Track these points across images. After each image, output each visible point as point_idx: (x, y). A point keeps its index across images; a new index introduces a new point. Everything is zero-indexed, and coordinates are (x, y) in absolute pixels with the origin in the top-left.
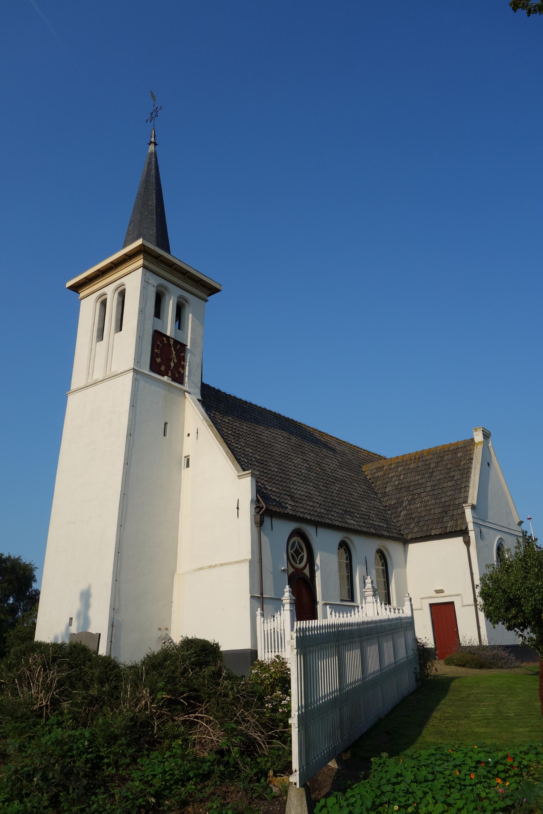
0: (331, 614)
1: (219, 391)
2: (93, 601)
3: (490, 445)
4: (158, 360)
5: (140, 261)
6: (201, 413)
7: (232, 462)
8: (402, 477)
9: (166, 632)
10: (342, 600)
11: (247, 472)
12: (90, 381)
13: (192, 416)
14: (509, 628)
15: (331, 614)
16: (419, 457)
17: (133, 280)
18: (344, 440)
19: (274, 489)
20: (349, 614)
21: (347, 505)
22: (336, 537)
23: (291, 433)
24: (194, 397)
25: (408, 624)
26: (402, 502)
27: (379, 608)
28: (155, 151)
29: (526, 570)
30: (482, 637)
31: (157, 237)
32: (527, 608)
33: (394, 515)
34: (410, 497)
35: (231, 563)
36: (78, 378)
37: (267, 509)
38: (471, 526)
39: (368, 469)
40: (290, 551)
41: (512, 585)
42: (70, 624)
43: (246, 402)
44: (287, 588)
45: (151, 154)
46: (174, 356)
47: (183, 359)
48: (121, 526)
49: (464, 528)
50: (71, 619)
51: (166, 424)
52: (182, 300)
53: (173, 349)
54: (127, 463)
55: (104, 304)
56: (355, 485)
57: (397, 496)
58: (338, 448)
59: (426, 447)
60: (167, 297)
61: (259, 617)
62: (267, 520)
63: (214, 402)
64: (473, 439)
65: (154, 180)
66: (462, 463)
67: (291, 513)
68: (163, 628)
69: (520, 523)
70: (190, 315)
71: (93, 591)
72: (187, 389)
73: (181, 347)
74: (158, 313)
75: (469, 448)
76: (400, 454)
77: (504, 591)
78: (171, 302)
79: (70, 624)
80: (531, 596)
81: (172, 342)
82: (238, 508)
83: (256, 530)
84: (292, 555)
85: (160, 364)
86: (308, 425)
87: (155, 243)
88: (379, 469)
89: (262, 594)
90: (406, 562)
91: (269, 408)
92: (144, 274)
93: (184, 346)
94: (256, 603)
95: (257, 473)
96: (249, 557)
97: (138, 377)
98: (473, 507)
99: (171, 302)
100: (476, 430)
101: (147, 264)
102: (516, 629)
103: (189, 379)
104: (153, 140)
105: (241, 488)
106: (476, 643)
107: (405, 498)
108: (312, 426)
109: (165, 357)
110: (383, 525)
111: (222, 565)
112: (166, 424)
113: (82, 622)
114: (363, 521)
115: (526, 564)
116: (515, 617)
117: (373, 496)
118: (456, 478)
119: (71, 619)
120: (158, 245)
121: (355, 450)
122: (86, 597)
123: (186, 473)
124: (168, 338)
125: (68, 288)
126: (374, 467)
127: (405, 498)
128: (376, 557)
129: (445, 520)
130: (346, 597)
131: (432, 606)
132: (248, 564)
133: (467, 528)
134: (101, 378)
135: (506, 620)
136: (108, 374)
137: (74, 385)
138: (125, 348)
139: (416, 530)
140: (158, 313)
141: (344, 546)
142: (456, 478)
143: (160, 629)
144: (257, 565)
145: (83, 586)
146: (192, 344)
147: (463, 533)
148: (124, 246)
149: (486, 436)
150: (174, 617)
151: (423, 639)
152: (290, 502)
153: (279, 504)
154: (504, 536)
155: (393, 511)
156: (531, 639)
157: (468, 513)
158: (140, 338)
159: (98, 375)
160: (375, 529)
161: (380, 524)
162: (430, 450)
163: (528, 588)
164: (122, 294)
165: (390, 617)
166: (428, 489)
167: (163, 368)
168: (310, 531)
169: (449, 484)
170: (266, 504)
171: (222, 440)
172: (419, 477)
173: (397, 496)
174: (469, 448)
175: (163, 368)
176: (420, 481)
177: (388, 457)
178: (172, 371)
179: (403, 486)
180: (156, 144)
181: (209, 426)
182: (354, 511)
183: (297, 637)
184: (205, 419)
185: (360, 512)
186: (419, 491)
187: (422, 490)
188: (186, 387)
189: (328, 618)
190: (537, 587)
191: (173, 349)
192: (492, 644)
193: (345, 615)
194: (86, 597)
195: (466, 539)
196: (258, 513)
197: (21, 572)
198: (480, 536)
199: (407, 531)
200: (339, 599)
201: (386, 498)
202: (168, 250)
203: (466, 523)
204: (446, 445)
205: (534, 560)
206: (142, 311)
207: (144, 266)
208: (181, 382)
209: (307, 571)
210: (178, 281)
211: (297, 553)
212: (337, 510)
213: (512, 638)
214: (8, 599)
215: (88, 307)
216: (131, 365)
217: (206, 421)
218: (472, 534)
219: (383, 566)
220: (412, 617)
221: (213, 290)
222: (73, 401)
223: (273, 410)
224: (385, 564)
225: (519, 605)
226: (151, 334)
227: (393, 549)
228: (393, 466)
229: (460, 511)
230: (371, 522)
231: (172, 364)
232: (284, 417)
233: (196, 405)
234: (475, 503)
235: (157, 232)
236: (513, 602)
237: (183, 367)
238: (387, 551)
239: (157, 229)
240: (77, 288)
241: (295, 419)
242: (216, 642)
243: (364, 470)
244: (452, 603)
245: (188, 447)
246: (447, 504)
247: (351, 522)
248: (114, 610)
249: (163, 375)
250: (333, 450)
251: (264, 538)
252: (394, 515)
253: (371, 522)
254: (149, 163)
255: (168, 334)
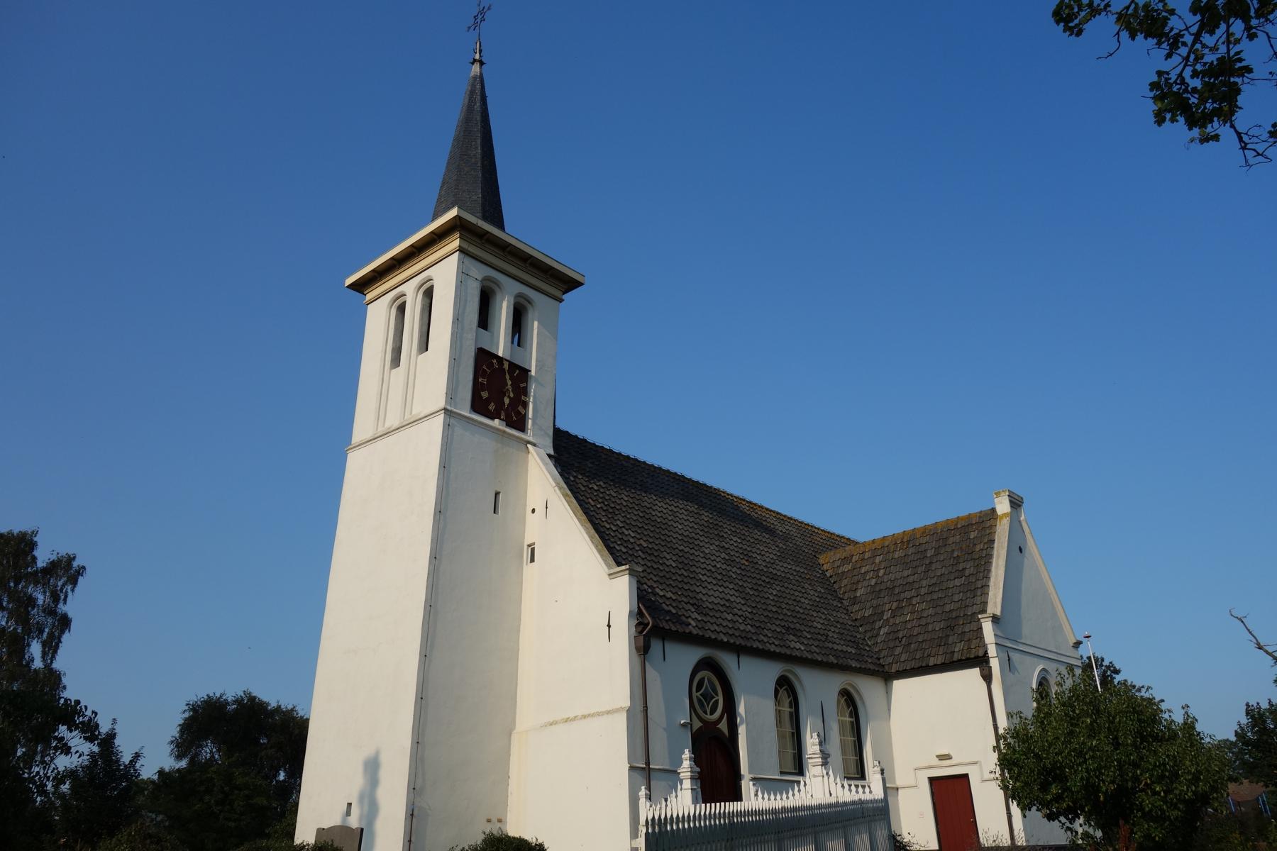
0: (756, 795)
1: (585, 441)
2: (384, 774)
3: (1022, 518)
4: (485, 395)
5: (454, 243)
6: (552, 476)
7: (599, 551)
8: (881, 573)
9: (499, 825)
10: (782, 773)
11: (623, 568)
12: (381, 430)
13: (539, 482)
14: (1051, 817)
15: (756, 795)
16: (908, 540)
17: (445, 271)
18: (789, 514)
19: (669, 595)
20: (784, 796)
21: (791, 619)
22: (769, 672)
23: (701, 505)
24: (542, 451)
25: (879, 813)
26: (883, 612)
27: (833, 785)
28: (481, 74)
29: (1073, 721)
30: (1016, 833)
31: (483, 206)
32: (1075, 783)
33: (869, 634)
34: (895, 605)
35: (599, 714)
36: (363, 426)
37: (654, 627)
38: (992, 651)
39: (827, 560)
40: (695, 694)
41: (1050, 745)
42: (348, 813)
43: (628, 457)
44: (687, 754)
45: (475, 78)
46: (509, 387)
47: (525, 392)
48: (425, 656)
49: (981, 654)
50: (350, 805)
51: (497, 494)
52: (522, 301)
53: (507, 377)
54: (435, 557)
55: (402, 309)
56: (806, 586)
57: (875, 603)
58: (779, 528)
59: (919, 524)
60: (498, 297)
61: (642, 801)
62: (656, 646)
63: (579, 463)
64: (993, 510)
65: (479, 118)
66: (978, 548)
67: (695, 632)
68: (494, 820)
69: (1077, 644)
70: (536, 324)
71: (384, 759)
72: (531, 439)
73: (521, 374)
74: (484, 320)
75: (988, 524)
76: (878, 536)
77: (1037, 756)
78: (505, 304)
79: (348, 813)
80: (1080, 764)
81: (506, 366)
82: (609, 626)
83: (637, 661)
84: (699, 701)
85: (488, 401)
86: (729, 491)
87: (479, 215)
88: (846, 560)
89: (648, 763)
90: (889, 710)
91: (665, 466)
92: (461, 263)
93: (525, 372)
94: (639, 778)
95: (640, 569)
96: (627, 704)
97: (453, 421)
98: (995, 619)
99: (505, 304)
100: (998, 494)
101: (465, 246)
102: (1062, 819)
103: (534, 423)
104: (477, 57)
105: (613, 593)
106: (1006, 841)
107: (887, 607)
108: (736, 494)
109: (495, 390)
110: (849, 650)
111: (585, 717)
112: (497, 494)
113: (366, 808)
114: (816, 643)
115: (1074, 711)
116: (1058, 798)
117: (835, 603)
118: (967, 573)
119: (350, 805)
120: (485, 218)
121: (807, 531)
122: (372, 767)
123: (529, 571)
124: (500, 360)
125: (351, 286)
126: (838, 556)
127: (887, 607)
128: (839, 702)
129: (951, 640)
130: (790, 767)
131: (933, 781)
132: (623, 718)
133: (986, 653)
134: (396, 425)
135: (1044, 805)
136: (408, 418)
137: (357, 437)
138: (432, 377)
139: (904, 657)
140: (484, 320)
141: (786, 688)
142: (967, 573)
143: (489, 821)
144: (640, 717)
145: (367, 752)
146: (539, 367)
147: (981, 661)
148: (435, 218)
149: (1016, 503)
150: (513, 800)
151: (905, 834)
152: (695, 615)
153: (677, 619)
154: (1051, 667)
155: (868, 627)
156: (1086, 835)
157: (988, 628)
158: (454, 361)
159: (393, 420)
160: (837, 657)
161: (845, 648)
162: (925, 527)
163: (1075, 750)
164: (429, 294)
165: (841, 800)
166: (923, 591)
167: (492, 407)
168: (728, 661)
169: (957, 582)
170: (653, 618)
171: (584, 517)
172: (909, 572)
173: (875, 603)
174: (988, 524)
175: (492, 407)
176: (911, 579)
177: (861, 539)
178: (506, 410)
179: (883, 587)
180: (482, 63)
181: (565, 496)
182: (802, 628)
183: (647, 833)
184: (558, 484)
185: (812, 630)
186: (908, 594)
187: (913, 593)
188: (529, 436)
189: (753, 800)
190: (1091, 748)
191: (507, 377)
192: (1032, 843)
193: (772, 797)
194: (372, 767)
195: (986, 672)
196: (641, 632)
197: (297, 731)
198: (1008, 665)
199: (890, 660)
200: (777, 770)
201: (857, 607)
202: (501, 226)
203: (985, 646)
204: (952, 521)
205: (1087, 704)
206: (457, 320)
207: (461, 250)
208: (522, 428)
209: (723, 725)
210: (516, 272)
211: (707, 697)
212: (774, 627)
213: (1055, 833)
214: (277, 774)
215: (378, 315)
216: (442, 404)
217: (560, 488)
218: (995, 664)
219: (851, 716)
220: (886, 799)
221: (570, 284)
222: (356, 461)
223: (673, 470)
224: (855, 714)
225: (1061, 779)
226: (473, 354)
227: (868, 689)
228: (867, 555)
229: (974, 626)
230: (830, 645)
231: (507, 401)
232: (690, 480)
233: (545, 464)
234: (998, 613)
235: (483, 197)
236: (1052, 775)
237: (525, 405)
238: (858, 692)
239: (483, 192)
240: (361, 286)
241: (709, 484)
242: (540, 841)
243: (821, 561)
244: (966, 776)
245: (533, 530)
246: (954, 615)
247: (796, 646)
248: (415, 789)
249: (492, 418)
250: (771, 532)
251: (652, 674)
252: (869, 634)
253: (830, 645)
254: (472, 92)
255: (500, 354)
